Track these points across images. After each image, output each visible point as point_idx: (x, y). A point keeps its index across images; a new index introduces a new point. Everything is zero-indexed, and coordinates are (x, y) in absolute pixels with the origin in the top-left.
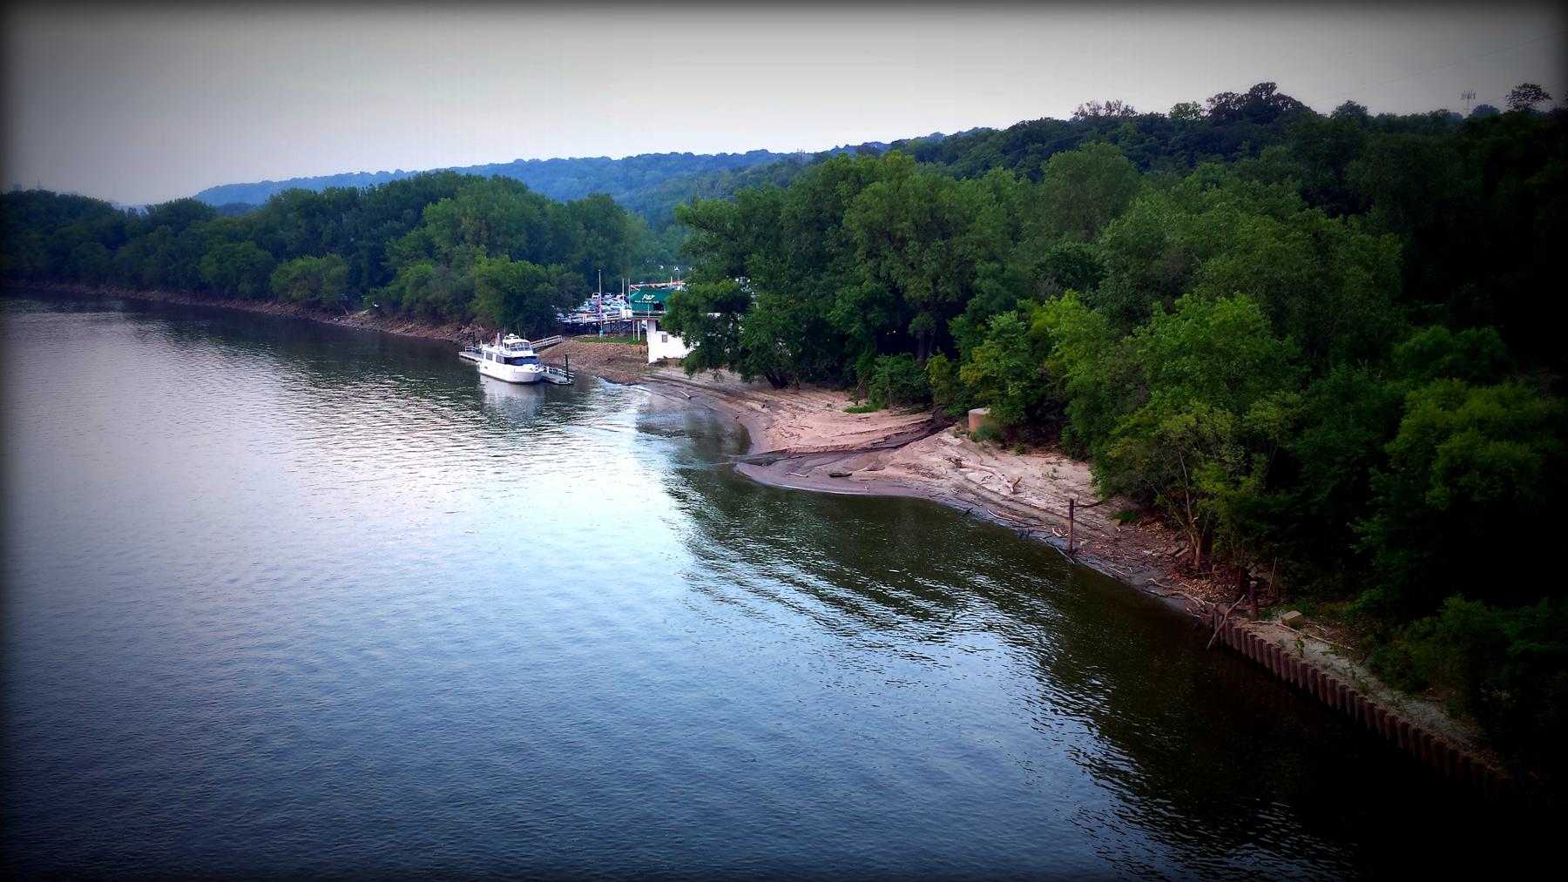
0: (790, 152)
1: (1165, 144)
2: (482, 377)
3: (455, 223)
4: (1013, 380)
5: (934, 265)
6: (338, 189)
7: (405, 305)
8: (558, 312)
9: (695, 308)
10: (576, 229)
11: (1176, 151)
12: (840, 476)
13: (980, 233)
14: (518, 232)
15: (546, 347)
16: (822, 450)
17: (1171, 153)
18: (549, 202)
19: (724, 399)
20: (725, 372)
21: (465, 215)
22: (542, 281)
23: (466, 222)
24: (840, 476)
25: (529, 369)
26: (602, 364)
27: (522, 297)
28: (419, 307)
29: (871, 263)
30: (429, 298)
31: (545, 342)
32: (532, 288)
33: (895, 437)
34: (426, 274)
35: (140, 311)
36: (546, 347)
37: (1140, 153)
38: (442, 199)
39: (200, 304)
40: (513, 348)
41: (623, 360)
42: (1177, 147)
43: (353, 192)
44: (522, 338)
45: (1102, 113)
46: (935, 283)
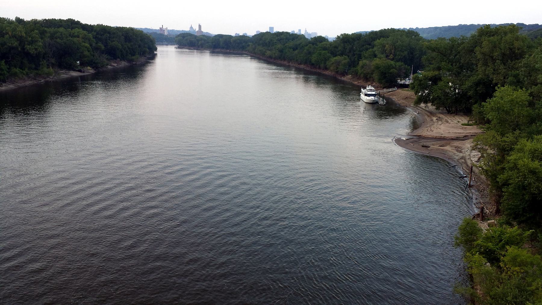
0: (464, 24)
12: (426, 147)
16: (435, 137)
18: (7, 33)
20: (429, 105)
22: (393, 68)
23: (387, 46)
27: (385, 73)
28: (362, 76)
29: (483, 68)
31: (391, 90)
33: (470, 136)
34: (365, 63)
35: (299, 71)
39: (312, 70)
40: (371, 90)
43: (361, 34)
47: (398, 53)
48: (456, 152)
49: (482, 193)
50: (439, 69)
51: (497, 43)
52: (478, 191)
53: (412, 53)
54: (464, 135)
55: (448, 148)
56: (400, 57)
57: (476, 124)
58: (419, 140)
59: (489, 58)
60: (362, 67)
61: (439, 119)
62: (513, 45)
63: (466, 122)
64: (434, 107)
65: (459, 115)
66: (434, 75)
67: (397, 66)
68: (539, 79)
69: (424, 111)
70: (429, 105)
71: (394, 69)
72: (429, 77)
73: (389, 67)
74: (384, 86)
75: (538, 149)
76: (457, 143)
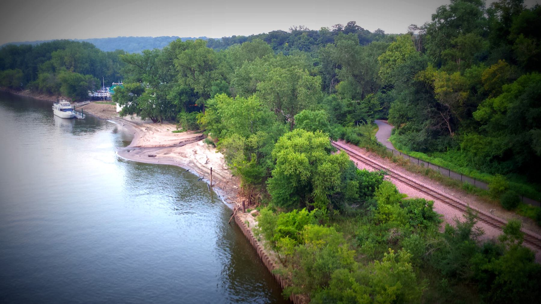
1: (316, 41)
2: (54, 116)
3: (62, 58)
4: (215, 123)
5: (203, 80)
6: (25, 45)
7: (40, 88)
8: (89, 92)
9: (123, 93)
10: (109, 62)
11: (319, 44)
12: (152, 156)
13: (221, 69)
14: (86, 62)
15: (84, 105)
16: (154, 146)
17: (318, 44)
19: (134, 126)
20: (135, 115)
21: (66, 56)
23: (66, 58)
24: (152, 156)
25: (69, 114)
26: (100, 112)
28: (44, 89)
30: (47, 86)
31: (83, 103)
32: (79, 83)
33: (184, 142)
36: (84, 105)
37: (307, 44)
38: (58, 50)
40: (66, 105)
41: (108, 111)
42: (319, 42)
44: (68, 101)
45: (298, 29)
46: (204, 87)
47: (79, 65)
48: (182, 158)
49: (225, 190)
50: (139, 80)
51: (193, 55)
52: (221, 189)
53: (92, 65)
54: (179, 141)
55: (172, 155)
56: (81, 69)
57: (185, 130)
58: (142, 151)
59: (187, 70)
60: (44, 80)
61: (147, 129)
62: (206, 57)
63: (175, 130)
64: (140, 118)
65: (164, 123)
66: (136, 87)
67: (87, 79)
68: (161, 88)
69: (128, 122)
70: (135, 115)
71: (84, 82)
72: (131, 89)
73: (79, 80)
74: (74, 100)
75: (298, 144)
76: (178, 149)
